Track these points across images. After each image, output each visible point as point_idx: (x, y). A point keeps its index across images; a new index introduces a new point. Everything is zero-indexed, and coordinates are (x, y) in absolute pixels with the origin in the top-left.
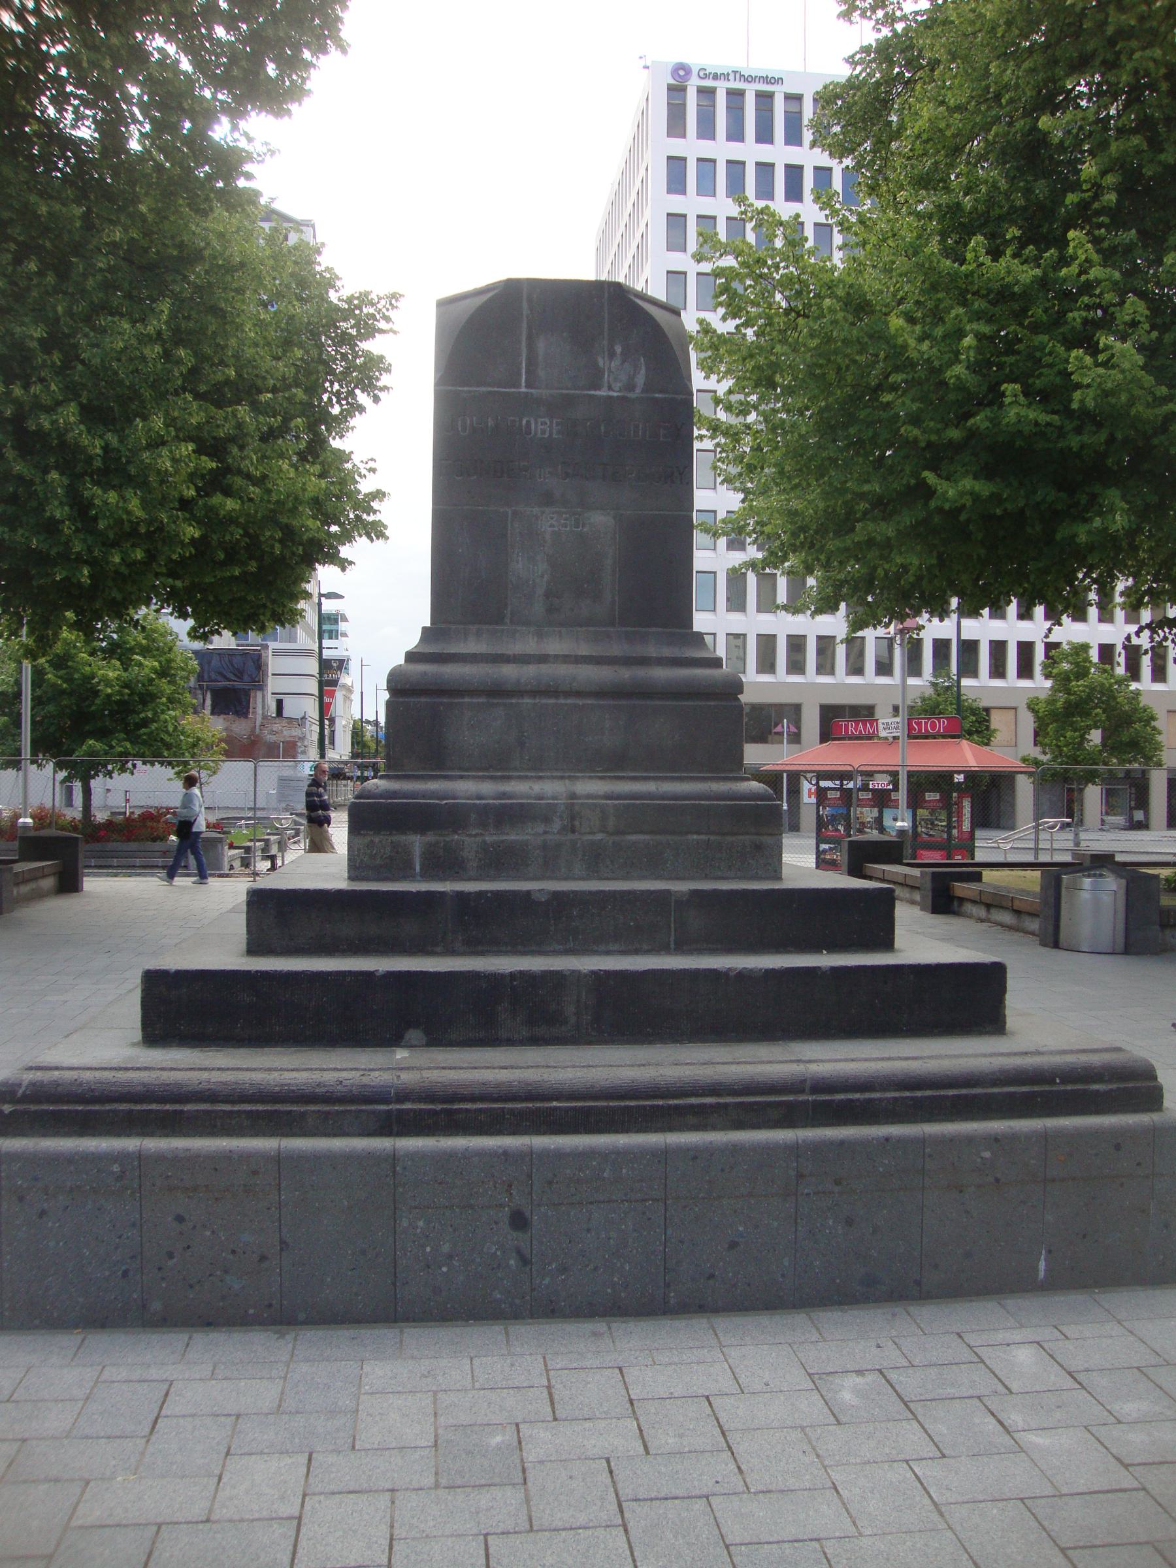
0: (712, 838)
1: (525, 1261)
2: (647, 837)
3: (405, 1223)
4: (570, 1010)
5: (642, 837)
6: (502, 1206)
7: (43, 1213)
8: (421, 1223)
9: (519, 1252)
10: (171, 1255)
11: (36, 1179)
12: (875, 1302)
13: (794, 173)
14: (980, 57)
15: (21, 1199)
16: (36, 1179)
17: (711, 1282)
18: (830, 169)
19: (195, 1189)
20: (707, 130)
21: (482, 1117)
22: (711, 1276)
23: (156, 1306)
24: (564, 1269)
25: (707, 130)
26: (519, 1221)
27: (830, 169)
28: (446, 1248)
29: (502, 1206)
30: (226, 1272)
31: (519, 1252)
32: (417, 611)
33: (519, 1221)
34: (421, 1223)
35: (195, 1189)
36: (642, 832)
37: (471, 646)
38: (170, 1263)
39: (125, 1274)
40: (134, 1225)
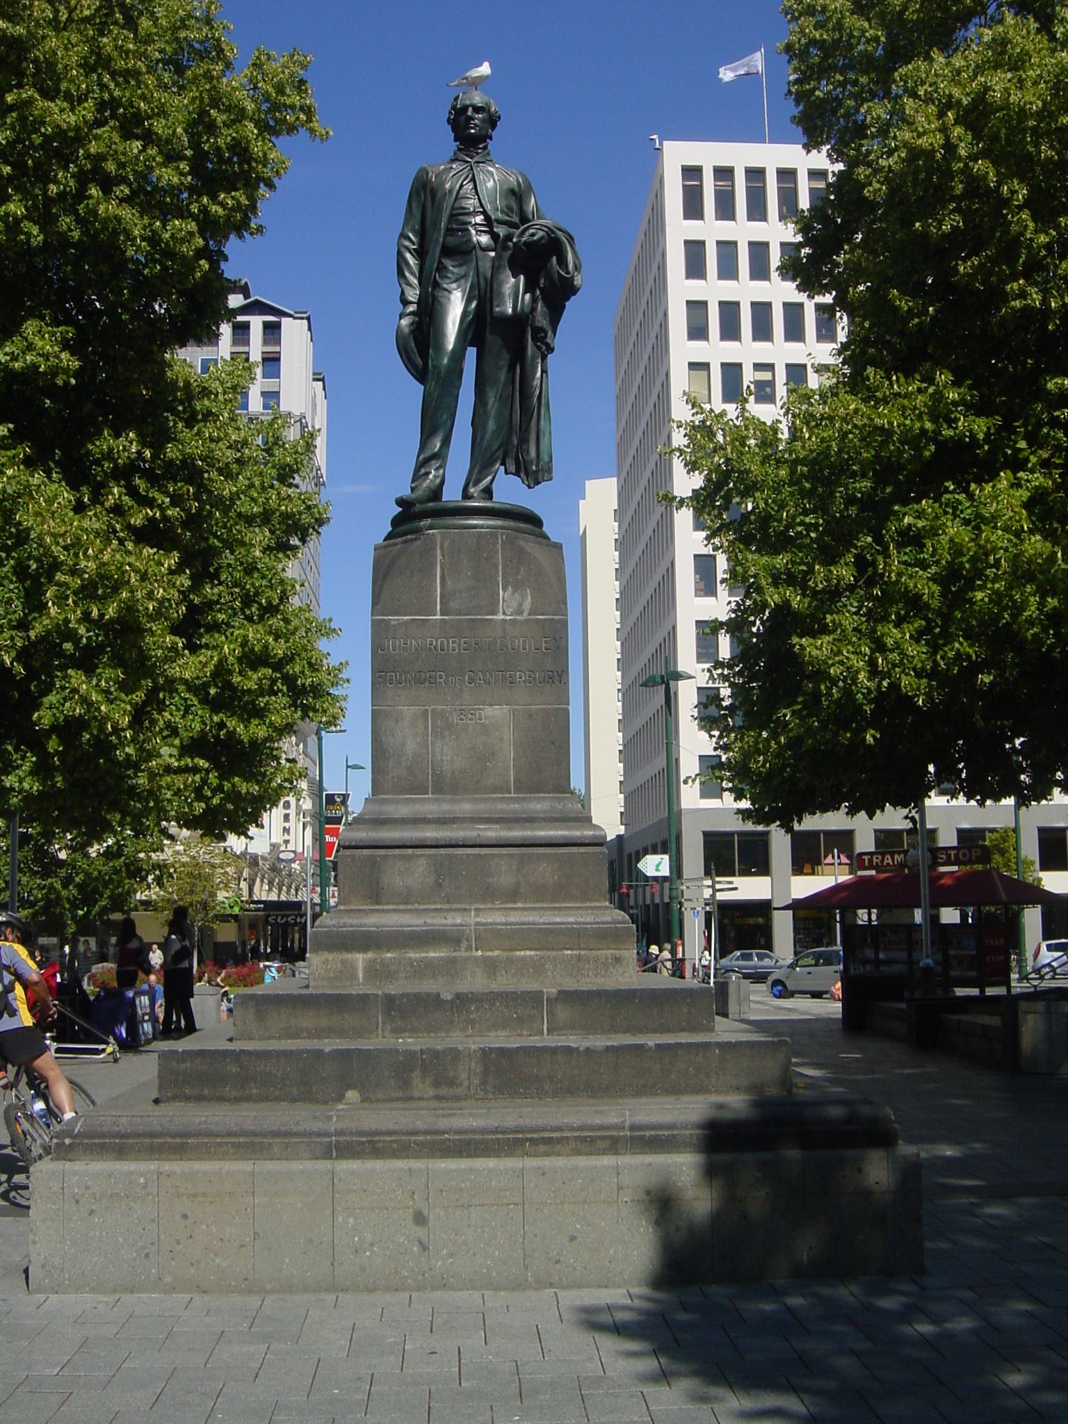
0: (583, 952)
1: (424, 1248)
2: (533, 953)
3: (340, 1219)
4: (464, 1076)
5: (528, 953)
6: (408, 1207)
7: (92, 1212)
8: (351, 1220)
9: (420, 1242)
10: (178, 1243)
11: (87, 1188)
12: (555, 1094)
13: (762, 310)
14: (323, 676)
15: (77, 1202)
16: (87, 1188)
17: (558, 1266)
18: (801, 305)
19: (195, 1195)
20: (726, 210)
21: (395, 1146)
22: (558, 1262)
23: (168, 1279)
24: (452, 1255)
25: (726, 210)
26: (420, 1219)
27: (801, 305)
28: (369, 1237)
29: (408, 1207)
30: (216, 1254)
31: (420, 1242)
32: (367, 790)
33: (420, 1219)
34: (351, 1220)
35: (195, 1195)
36: (531, 949)
37: (403, 811)
38: (178, 1248)
39: (147, 1256)
40: (153, 1221)
